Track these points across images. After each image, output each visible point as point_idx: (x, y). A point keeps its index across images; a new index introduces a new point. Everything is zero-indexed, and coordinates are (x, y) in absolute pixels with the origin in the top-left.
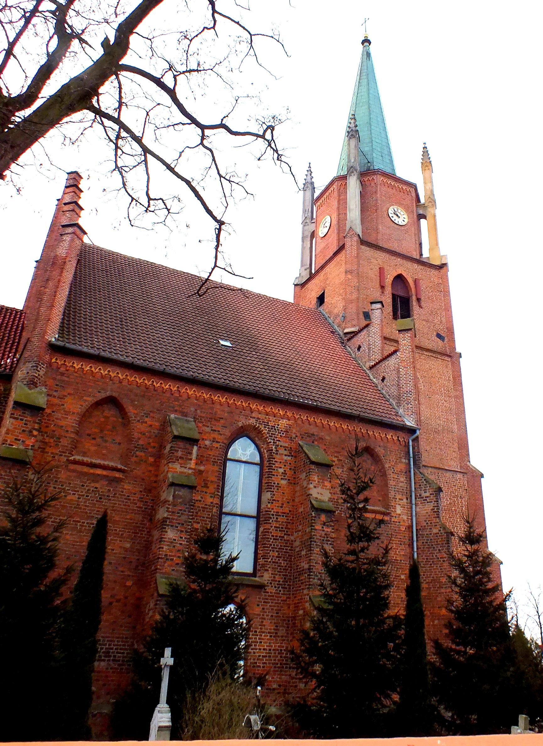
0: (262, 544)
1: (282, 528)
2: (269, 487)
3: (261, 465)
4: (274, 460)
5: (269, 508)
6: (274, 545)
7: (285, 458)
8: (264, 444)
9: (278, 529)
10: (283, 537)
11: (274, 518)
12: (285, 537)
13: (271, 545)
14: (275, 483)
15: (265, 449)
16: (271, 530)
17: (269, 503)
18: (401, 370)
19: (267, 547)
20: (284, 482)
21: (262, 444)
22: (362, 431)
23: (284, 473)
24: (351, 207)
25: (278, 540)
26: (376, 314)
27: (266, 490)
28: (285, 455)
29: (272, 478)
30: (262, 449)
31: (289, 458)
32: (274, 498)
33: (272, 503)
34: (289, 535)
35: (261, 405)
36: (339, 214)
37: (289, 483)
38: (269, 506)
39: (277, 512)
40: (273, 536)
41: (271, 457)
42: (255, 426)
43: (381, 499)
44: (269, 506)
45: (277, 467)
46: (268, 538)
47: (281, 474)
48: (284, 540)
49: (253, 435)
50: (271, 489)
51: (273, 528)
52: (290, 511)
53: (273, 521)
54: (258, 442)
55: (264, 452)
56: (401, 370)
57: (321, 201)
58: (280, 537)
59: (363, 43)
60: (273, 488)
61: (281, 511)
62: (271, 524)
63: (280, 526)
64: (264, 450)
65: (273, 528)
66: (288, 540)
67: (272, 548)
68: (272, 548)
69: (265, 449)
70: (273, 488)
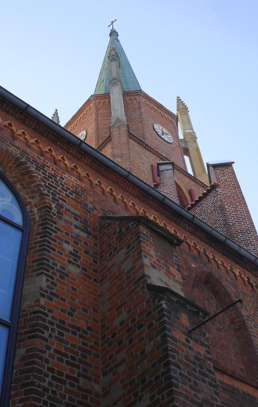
0: (23, 386)
1: (73, 358)
2: (42, 266)
3: (24, 229)
4: (54, 225)
5: (42, 307)
6: (54, 392)
7: (77, 231)
8: (32, 198)
9: (65, 359)
10: (77, 381)
11: (53, 330)
12: (82, 380)
13: (46, 390)
14: (56, 265)
15: (36, 206)
16: (46, 356)
17: (43, 296)
18: (226, 207)
19: (37, 392)
20: (72, 268)
21: (30, 198)
22: (197, 247)
23: (74, 255)
24: (116, 108)
25: (64, 382)
26: (167, 175)
27: (35, 273)
28: (75, 226)
29: (49, 252)
30: (28, 207)
31: (83, 234)
32: (54, 291)
33: (51, 299)
34: (90, 379)
35: (32, 138)
36: (98, 124)
37: (84, 274)
38: (43, 301)
39: (61, 321)
40: (50, 369)
41: (46, 220)
42: (18, 159)
43: (243, 367)
44: (43, 301)
45: (60, 239)
46: (40, 372)
47: (67, 253)
48: (79, 388)
49: (11, 176)
50: (48, 271)
51: (52, 351)
52: (89, 328)
53: (50, 336)
54: (21, 193)
55: (31, 212)
56: (226, 207)
57: (72, 126)
58: (68, 377)
59: (111, 35)
60: (51, 271)
61: (70, 322)
62: (46, 340)
63: (70, 354)
64: (32, 207)
65: (52, 351)
66: (89, 391)
67: (49, 397)
68: (49, 397)
69: (36, 206)
70: (51, 271)
